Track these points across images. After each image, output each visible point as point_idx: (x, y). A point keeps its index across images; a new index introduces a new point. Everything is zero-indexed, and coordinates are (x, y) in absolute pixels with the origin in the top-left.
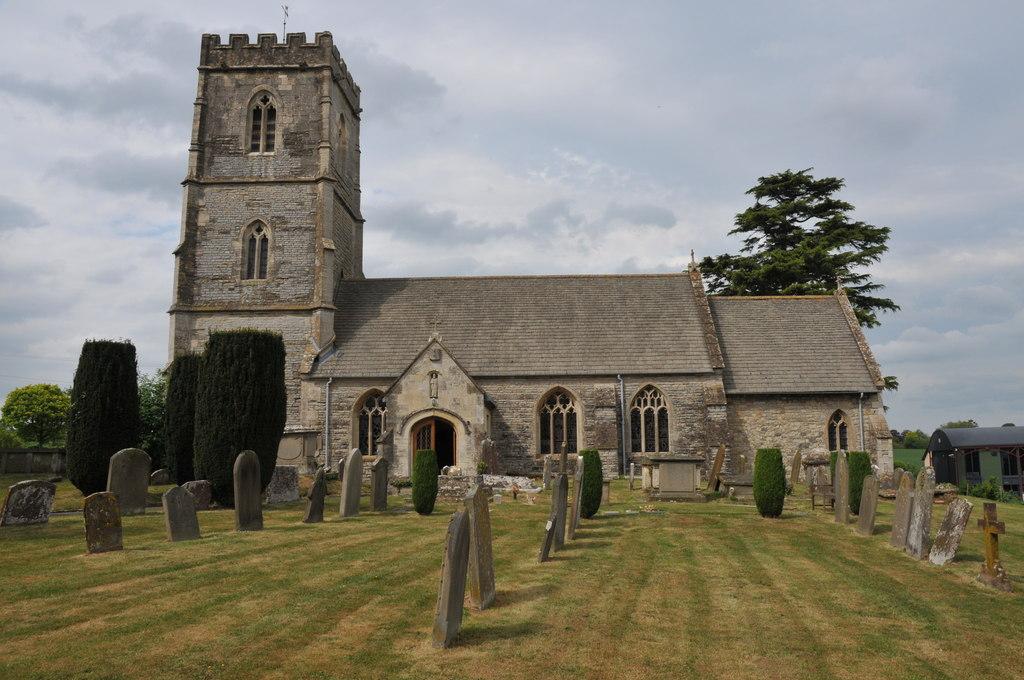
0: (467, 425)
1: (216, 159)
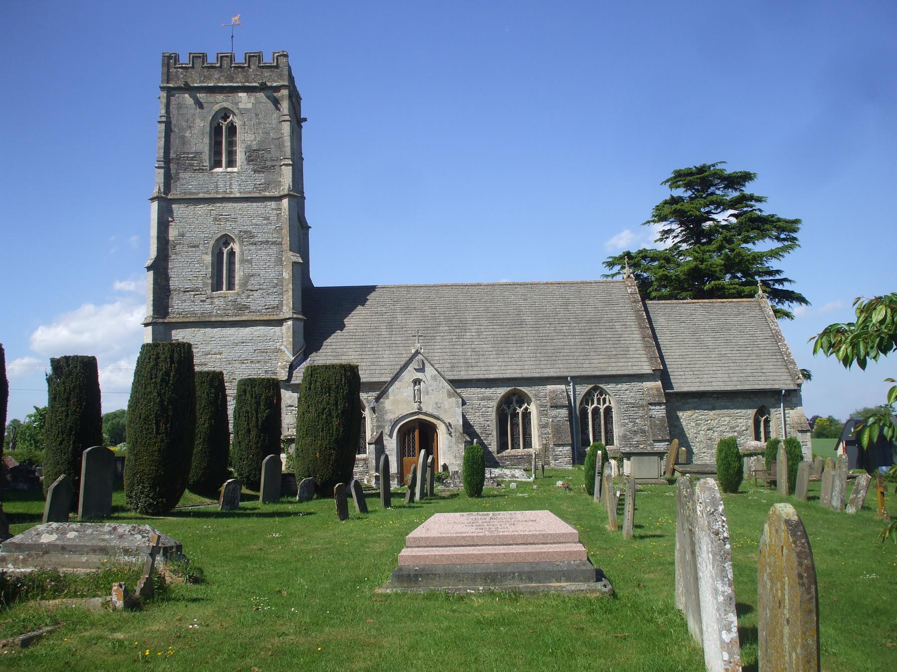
0: (449, 426)
1: (181, 175)
